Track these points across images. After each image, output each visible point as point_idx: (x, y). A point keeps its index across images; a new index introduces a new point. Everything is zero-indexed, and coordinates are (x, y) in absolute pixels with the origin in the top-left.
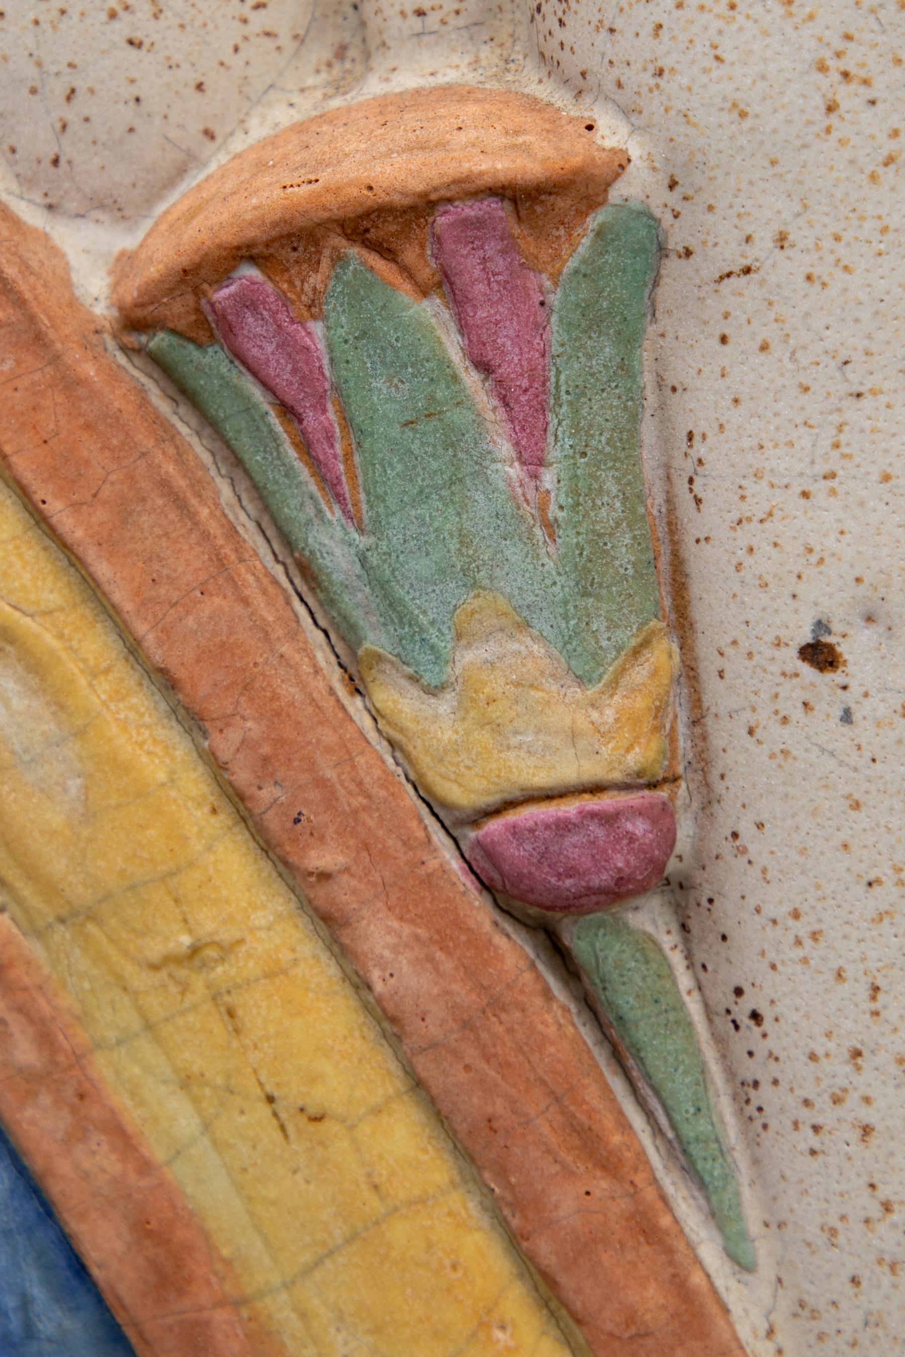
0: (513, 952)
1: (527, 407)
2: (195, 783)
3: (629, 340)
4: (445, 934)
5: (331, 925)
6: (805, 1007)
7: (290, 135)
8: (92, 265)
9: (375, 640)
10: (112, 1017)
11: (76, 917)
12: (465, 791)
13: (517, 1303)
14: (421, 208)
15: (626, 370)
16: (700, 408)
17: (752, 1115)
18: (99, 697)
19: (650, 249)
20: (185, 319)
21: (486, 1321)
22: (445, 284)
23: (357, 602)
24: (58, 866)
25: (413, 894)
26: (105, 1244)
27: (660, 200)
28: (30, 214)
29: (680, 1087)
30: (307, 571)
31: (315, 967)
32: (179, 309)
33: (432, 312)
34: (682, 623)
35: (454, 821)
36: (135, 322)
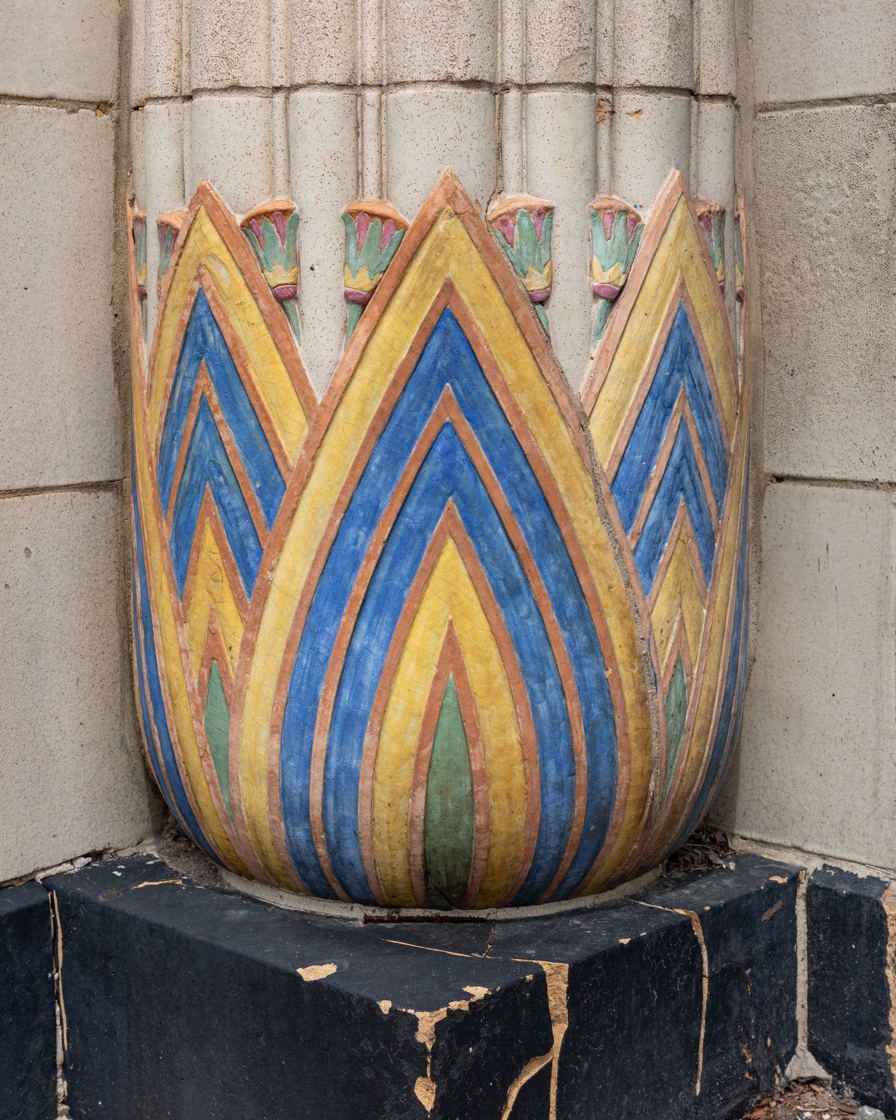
0: (277, 305)
1: (283, 237)
2: (243, 282)
3: (295, 230)
4: (269, 301)
5: (256, 299)
6: (309, 312)
7: (265, 204)
8: (239, 219)
9: (265, 266)
10: (232, 312)
11: (228, 299)
12: (273, 285)
13: (274, 348)
14: (272, 212)
15: (295, 234)
16: (302, 239)
17: (303, 327)
18: (525, 528)
19: (297, 219)
20: (247, 225)
21: (270, 350)
22: (274, 222)
23: (263, 261)
24: (227, 292)
25: (266, 296)
26: (229, 340)
27: (299, 213)
28: (232, 213)
29: (295, 323)
30: (258, 257)
31: (255, 306)
32: (246, 224)
33: (273, 225)
34: (299, 265)
35: (272, 288)
36: (242, 226)
